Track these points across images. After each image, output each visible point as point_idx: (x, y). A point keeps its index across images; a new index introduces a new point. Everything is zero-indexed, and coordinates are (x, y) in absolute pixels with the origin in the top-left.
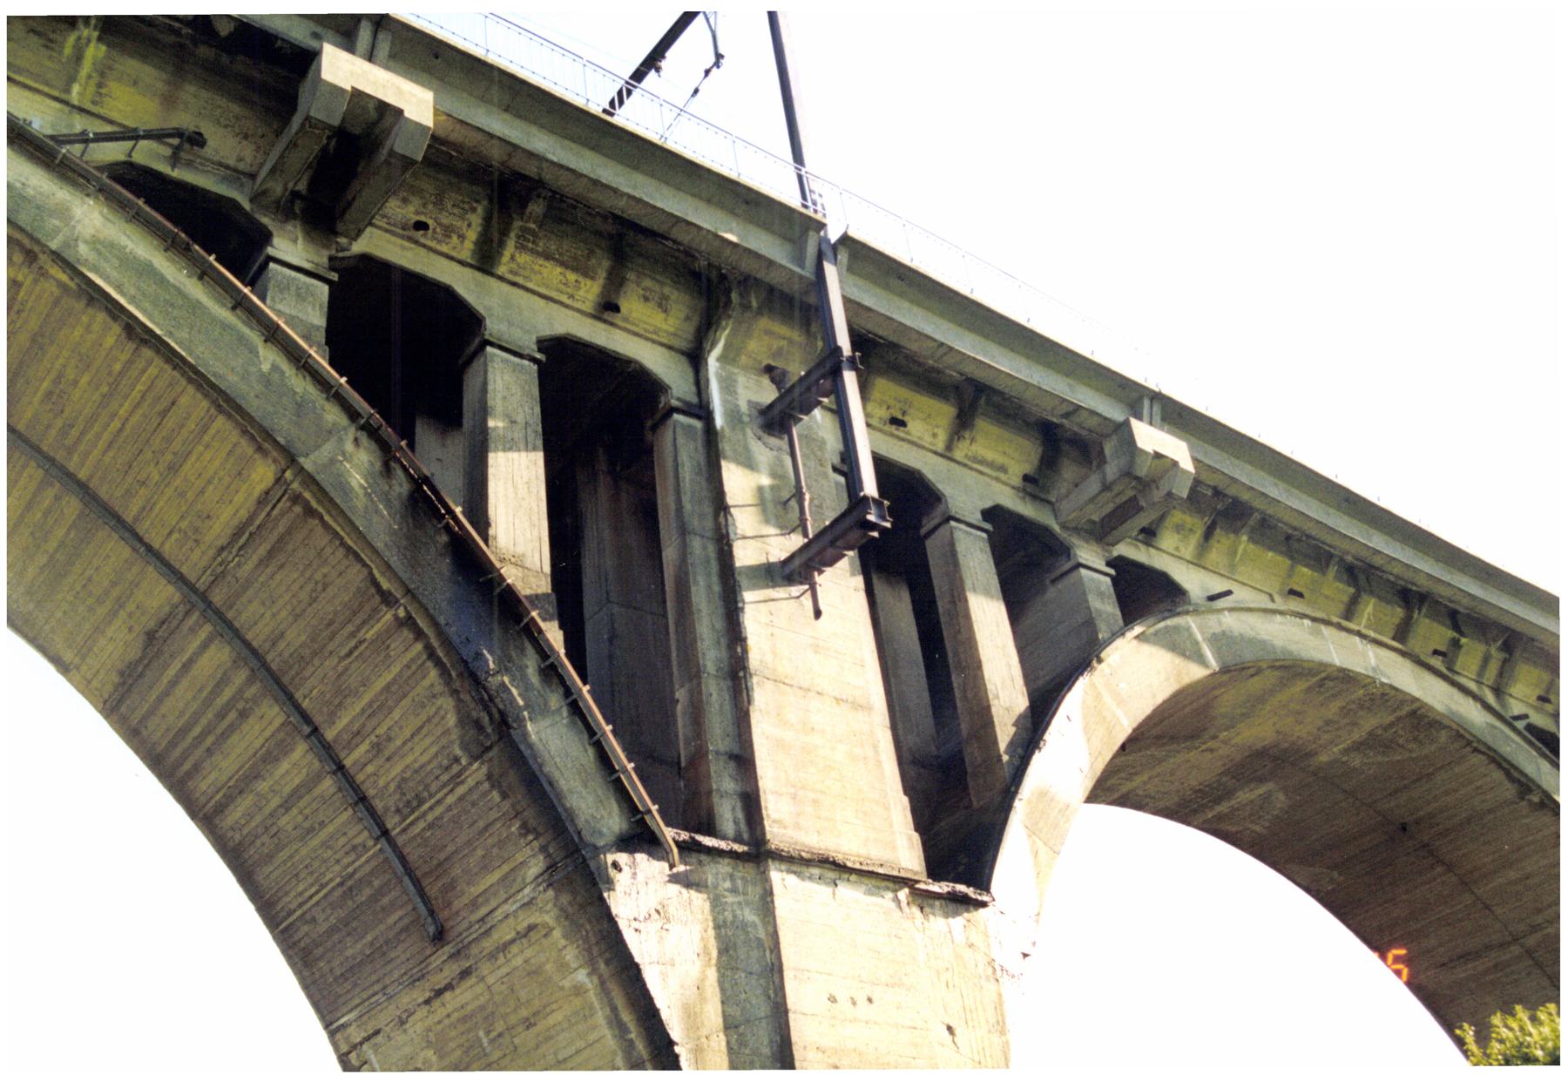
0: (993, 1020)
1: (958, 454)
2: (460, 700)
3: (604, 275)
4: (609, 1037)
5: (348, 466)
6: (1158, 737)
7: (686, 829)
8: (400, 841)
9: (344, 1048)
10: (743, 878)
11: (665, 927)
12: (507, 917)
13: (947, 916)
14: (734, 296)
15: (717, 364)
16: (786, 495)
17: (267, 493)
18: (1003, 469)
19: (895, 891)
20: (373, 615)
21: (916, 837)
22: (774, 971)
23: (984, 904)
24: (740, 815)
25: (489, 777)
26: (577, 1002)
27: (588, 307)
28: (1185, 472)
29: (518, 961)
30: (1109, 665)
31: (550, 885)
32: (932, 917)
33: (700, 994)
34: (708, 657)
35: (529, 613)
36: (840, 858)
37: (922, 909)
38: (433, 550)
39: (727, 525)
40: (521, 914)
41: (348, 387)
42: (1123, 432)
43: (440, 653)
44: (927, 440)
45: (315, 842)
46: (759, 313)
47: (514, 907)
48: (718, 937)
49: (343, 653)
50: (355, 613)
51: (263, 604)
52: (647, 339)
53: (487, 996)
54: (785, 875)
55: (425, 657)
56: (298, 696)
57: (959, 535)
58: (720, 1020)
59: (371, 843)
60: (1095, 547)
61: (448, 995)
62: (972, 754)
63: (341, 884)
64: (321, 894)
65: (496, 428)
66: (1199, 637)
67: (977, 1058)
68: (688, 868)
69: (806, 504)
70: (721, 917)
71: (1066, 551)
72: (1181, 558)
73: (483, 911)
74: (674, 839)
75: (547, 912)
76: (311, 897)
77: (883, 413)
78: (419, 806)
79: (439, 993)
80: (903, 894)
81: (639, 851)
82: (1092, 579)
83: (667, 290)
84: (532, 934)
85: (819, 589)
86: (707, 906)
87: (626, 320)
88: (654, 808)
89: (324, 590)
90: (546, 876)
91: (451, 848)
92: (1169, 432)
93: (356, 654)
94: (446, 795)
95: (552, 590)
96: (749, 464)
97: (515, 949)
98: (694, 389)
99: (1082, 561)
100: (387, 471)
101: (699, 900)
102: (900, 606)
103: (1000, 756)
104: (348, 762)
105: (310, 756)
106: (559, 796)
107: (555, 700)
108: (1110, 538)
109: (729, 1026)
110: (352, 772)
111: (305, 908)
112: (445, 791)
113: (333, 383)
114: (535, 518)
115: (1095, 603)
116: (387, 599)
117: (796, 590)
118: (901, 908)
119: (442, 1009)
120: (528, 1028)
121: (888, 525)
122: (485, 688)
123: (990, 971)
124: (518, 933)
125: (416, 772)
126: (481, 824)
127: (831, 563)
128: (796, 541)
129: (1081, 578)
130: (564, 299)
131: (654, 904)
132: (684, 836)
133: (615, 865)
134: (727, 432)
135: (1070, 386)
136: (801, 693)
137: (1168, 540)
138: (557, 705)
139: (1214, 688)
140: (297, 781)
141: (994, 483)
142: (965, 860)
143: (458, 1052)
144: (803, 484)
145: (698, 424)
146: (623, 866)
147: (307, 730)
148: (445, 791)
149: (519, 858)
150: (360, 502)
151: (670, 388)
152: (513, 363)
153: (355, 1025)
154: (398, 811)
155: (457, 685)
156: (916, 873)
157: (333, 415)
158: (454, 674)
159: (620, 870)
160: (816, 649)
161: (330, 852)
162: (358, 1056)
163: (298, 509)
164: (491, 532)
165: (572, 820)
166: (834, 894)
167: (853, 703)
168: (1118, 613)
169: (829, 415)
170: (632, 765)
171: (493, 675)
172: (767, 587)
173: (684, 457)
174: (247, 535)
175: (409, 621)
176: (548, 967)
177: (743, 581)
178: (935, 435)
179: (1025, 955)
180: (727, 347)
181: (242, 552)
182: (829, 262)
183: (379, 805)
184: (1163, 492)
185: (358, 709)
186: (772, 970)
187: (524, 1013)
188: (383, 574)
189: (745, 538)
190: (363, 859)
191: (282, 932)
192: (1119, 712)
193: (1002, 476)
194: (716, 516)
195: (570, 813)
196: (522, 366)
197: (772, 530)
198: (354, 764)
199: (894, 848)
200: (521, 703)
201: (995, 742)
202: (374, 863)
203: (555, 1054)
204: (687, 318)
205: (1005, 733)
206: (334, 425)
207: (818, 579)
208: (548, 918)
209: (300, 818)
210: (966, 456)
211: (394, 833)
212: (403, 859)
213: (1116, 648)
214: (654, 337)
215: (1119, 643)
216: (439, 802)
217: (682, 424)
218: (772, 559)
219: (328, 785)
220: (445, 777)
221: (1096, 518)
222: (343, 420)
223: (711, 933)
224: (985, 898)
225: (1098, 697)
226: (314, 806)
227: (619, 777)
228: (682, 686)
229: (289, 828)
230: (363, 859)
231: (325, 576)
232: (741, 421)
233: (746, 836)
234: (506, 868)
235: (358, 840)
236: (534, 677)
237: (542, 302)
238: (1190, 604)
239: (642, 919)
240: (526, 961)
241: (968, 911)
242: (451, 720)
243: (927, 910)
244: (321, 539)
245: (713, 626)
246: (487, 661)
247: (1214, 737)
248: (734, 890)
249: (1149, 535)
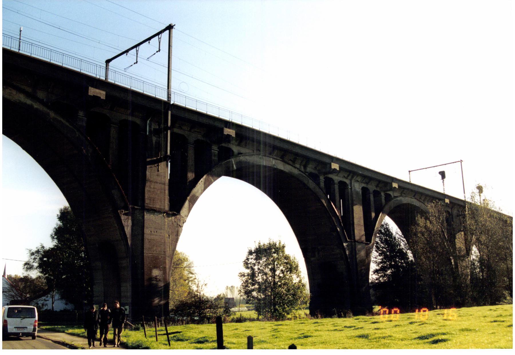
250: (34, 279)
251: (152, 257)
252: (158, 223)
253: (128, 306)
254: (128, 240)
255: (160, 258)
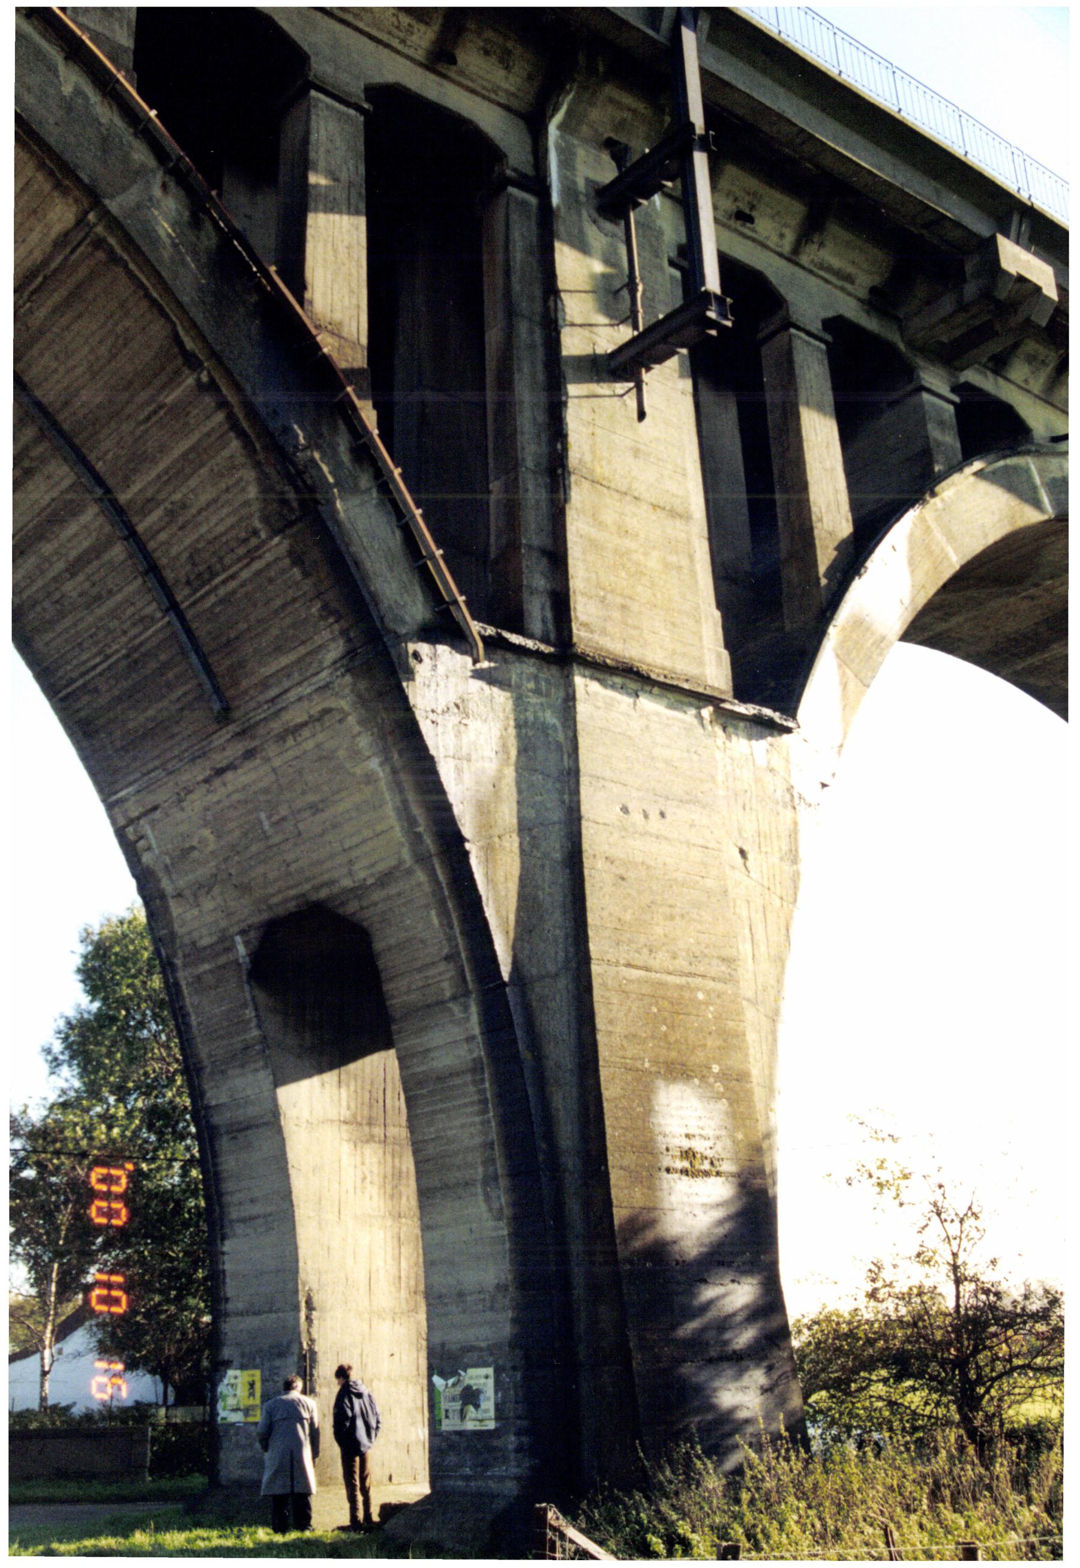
0: (785, 848)
1: (804, 259)
2: (262, 472)
3: (440, 21)
4: (398, 829)
5: (156, 213)
6: (982, 579)
7: (490, 623)
8: (189, 615)
9: (122, 822)
10: (547, 681)
11: (464, 721)
12: (300, 699)
13: (750, 737)
14: (581, 58)
15: (558, 133)
16: (617, 284)
17: (66, 234)
18: (849, 279)
19: (699, 708)
20: (175, 378)
21: (725, 654)
22: (571, 777)
23: (788, 730)
24: (549, 615)
25: (290, 553)
26: (368, 790)
27: (420, 55)
28: (1048, 299)
29: (310, 745)
30: (943, 500)
31: (348, 671)
32: (734, 738)
33: (496, 793)
34: (527, 451)
35: (344, 388)
36: (644, 669)
37: (724, 729)
38: (242, 310)
39: (556, 310)
40: (316, 698)
41: (157, 121)
42: (990, 249)
43: (245, 425)
44: (773, 241)
45: (100, 611)
46: (606, 79)
47: (308, 690)
48: (519, 736)
49: (141, 417)
50: (155, 375)
51: (56, 358)
52: (484, 97)
53: (273, 777)
54: (588, 681)
55: (226, 427)
56: (92, 457)
57: (797, 344)
58: (515, 821)
59: (159, 615)
60: (942, 372)
61: (229, 776)
62: (791, 574)
63: (127, 656)
64: (105, 665)
65: (317, 186)
66: (1037, 480)
67: (766, 883)
68: (492, 665)
69: (639, 295)
70: (522, 717)
71: (909, 373)
72: (1028, 391)
73: (272, 693)
74: (479, 633)
75: (344, 697)
76: (95, 667)
77: (728, 205)
78: (209, 581)
79: (220, 772)
80: (707, 712)
81: (440, 643)
82: (933, 405)
83: (510, 45)
84: (326, 718)
85: (645, 387)
86: (510, 704)
87: (462, 73)
88: (461, 599)
89: (125, 345)
90: (345, 661)
91: (243, 626)
92: (1035, 254)
93: (154, 419)
94: (241, 569)
95: (369, 364)
96: (582, 246)
97: (306, 732)
98: (530, 158)
99: (927, 385)
100: (195, 223)
101: (502, 698)
102: (728, 419)
103: (818, 579)
104: (140, 528)
105: (101, 519)
106: (365, 578)
107: (365, 480)
108: (957, 363)
109: (524, 828)
110: (143, 538)
111: (87, 677)
112: (240, 565)
113: (141, 115)
114: (354, 285)
115: (935, 433)
116: (192, 362)
117: (620, 387)
118: (703, 726)
119: (223, 790)
120: (314, 814)
121: (729, 324)
122: (293, 463)
123: (788, 797)
124: (310, 717)
125: (209, 543)
126: (278, 602)
127: (660, 360)
128: (625, 333)
129: (921, 405)
130: (395, 43)
131: (453, 698)
132: (490, 631)
133: (416, 656)
134: (563, 212)
135: (937, 192)
136: (617, 496)
137: (1019, 371)
138: (368, 485)
139: (1047, 536)
140: (86, 544)
141: (838, 293)
142: (773, 684)
143: (237, 833)
144: (637, 273)
145: (533, 200)
146: (424, 657)
147: (99, 492)
148: (240, 565)
149: (318, 640)
150: (167, 253)
151: (506, 156)
152: (338, 112)
153: (133, 799)
154: (188, 583)
155: (261, 456)
156: (722, 692)
157: (141, 155)
158: (258, 446)
159: (421, 661)
160: (636, 453)
161: (116, 623)
162: (135, 831)
163: (101, 255)
164: (308, 295)
165: (376, 605)
166: (635, 704)
167: (671, 511)
168: (958, 445)
169: (668, 203)
170: (441, 552)
171: (302, 450)
172: (591, 381)
173: (516, 235)
174: (40, 279)
175: (212, 387)
176: (341, 753)
177: (569, 373)
178: (782, 236)
179: (824, 785)
180: (569, 114)
181: (34, 298)
182: (688, 27)
183: (169, 575)
184: (1020, 317)
185: (153, 474)
186: (569, 774)
187: (311, 798)
188: (187, 333)
189: (573, 325)
190: (150, 632)
191: (62, 700)
192: (950, 550)
193: (848, 286)
194: (545, 301)
195: (374, 596)
196: (348, 116)
197: (602, 319)
198: (146, 530)
199: (701, 663)
200: (331, 480)
201: (815, 565)
202: (161, 636)
203: (341, 842)
204: (530, 77)
205: (825, 557)
206: (142, 165)
207: (646, 376)
208: (344, 704)
209: (87, 584)
210: (812, 261)
211: (183, 606)
212: (189, 632)
213: (953, 484)
214: (493, 96)
215: (956, 477)
216: (232, 577)
217: (516, 199)
218: (600, 351)
219: (118, 551)
220: (241, 551)
221: (945, 339)
222: (152, 162)
223: (512, 731)
224: (790, 724)
225: (928, 530)
226: (103, 573)
227: (426, 565)
228: (497, 479)
229: (74, 594)
230: (150, 632)
231: (127, 330)
232: (577, 201)
233: (552, 636)
234: (302, 650)
235: (148, 611)
236: (346, 458)
237: (371, 45)
238: (1032, 443)
239: (439, 711)
240: (318, 746)
241: (772, 735)
242: (253, 492)
243: (730, 729)
244: (124, 288)
245: (535, 419)
246: (297, 436)
247: (1037, 585)
248: (537, 692)
249: (999, 365)
250: (153, 1372)
251: (646, 989)
252: (666, 762)
253: (490, 1371)
254: (466, 854)
255: (707, 1004)
